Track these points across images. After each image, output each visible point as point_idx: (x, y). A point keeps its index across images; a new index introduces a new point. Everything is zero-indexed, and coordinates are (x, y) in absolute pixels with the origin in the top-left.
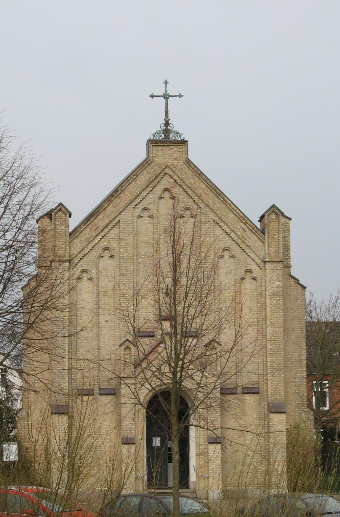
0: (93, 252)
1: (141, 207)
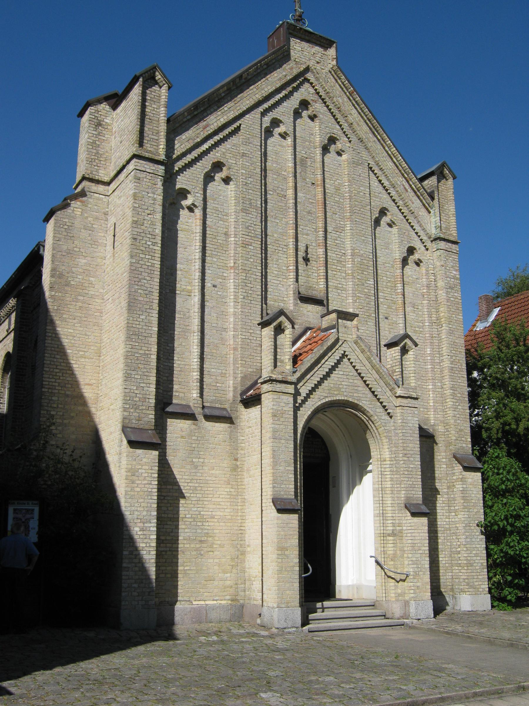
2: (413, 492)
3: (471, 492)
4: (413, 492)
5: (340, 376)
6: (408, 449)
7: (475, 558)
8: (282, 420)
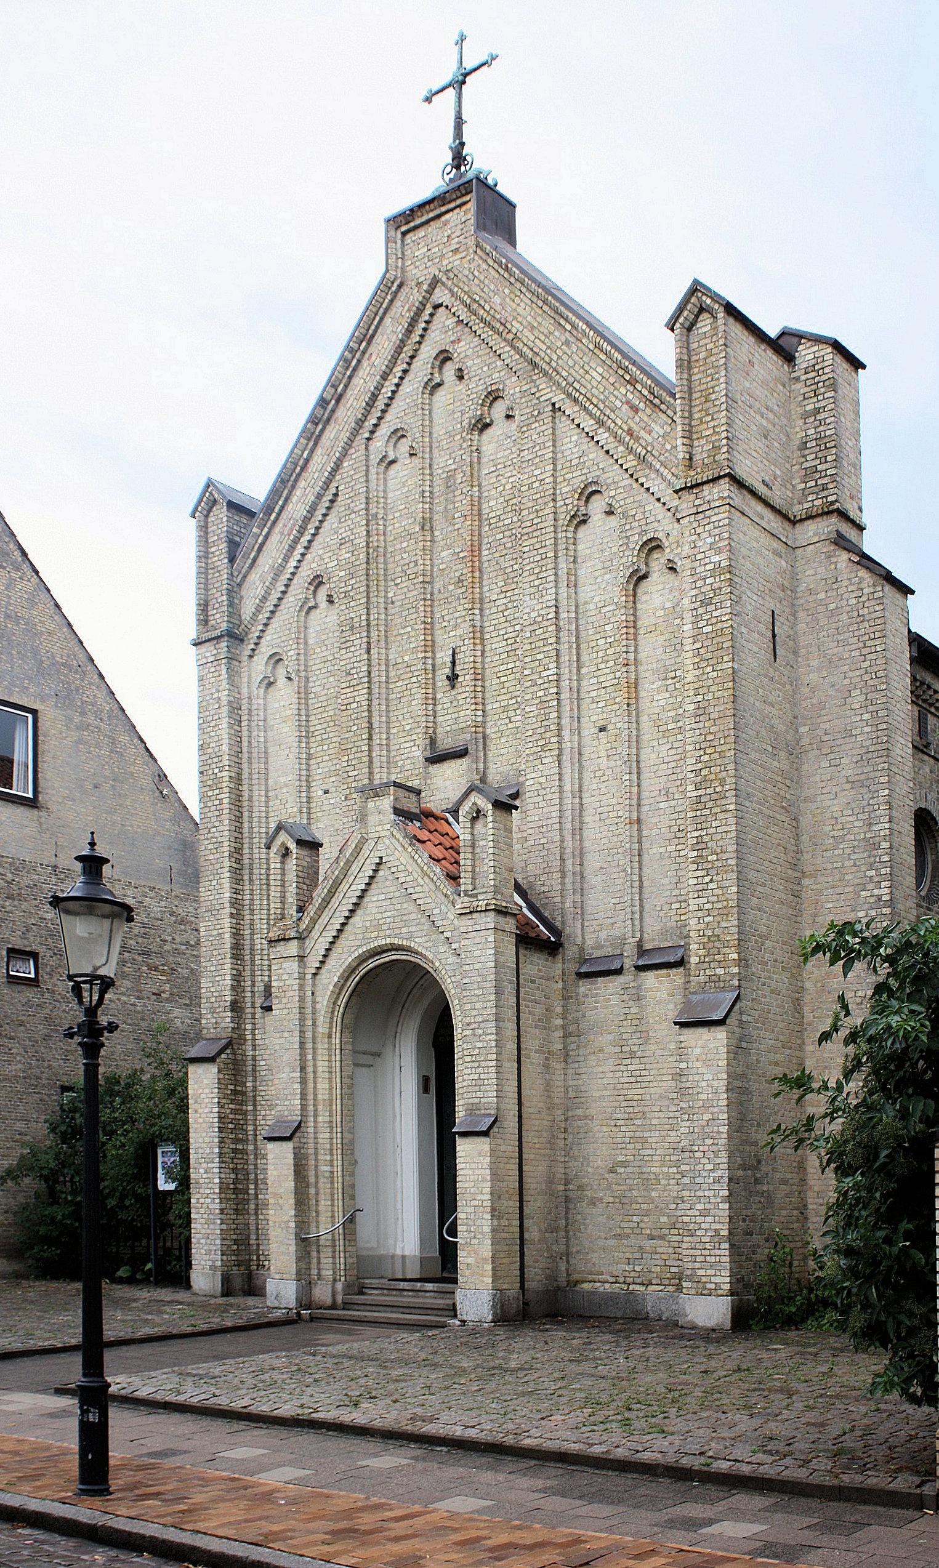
0: (289, 599)
1: (384, 430)
2: (479, 1094)
3: (697, 1078)
4: (479, 1094)
5: (380, 904)
6: (474, 1013)
7: (699, 1219)
8: (285, 1000)
